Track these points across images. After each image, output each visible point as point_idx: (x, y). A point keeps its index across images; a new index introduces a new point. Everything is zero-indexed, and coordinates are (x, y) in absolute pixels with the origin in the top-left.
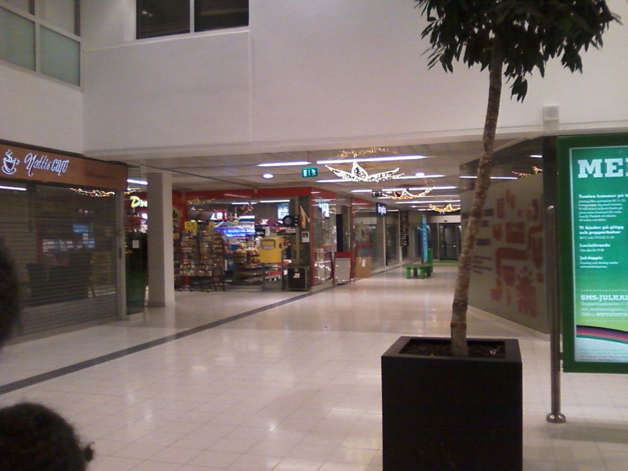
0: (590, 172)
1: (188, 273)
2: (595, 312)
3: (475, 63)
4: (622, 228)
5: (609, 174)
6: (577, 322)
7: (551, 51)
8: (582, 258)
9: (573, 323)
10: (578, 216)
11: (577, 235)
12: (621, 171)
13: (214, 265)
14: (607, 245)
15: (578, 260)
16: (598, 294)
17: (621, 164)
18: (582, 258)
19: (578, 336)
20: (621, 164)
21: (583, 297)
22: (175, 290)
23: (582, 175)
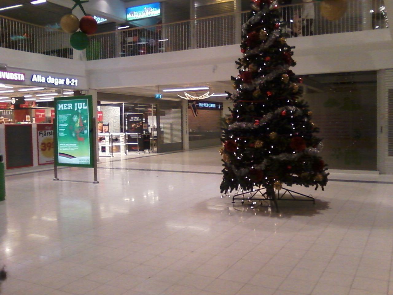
0: (61, 108)
1: (265, 46)
2: (62, 149)
3: (234, 107)
4: (67, 124)
5: (65, 109)
6: (59, 152)
7: (285, 45)
8: (60, 133)
9: (58, 153)
10: (63, 104)
11: (59, 126)
12: (67, 108)
13: (143, 52)
14: (64, 129)
15: (59, 134)
16: (63, 144)
17: (67, 106)
18: (60, 133)
19: (59, 156)
20: (67, 106)
21: (60, 145)
22: (361, 30)
23: (59, 109)
